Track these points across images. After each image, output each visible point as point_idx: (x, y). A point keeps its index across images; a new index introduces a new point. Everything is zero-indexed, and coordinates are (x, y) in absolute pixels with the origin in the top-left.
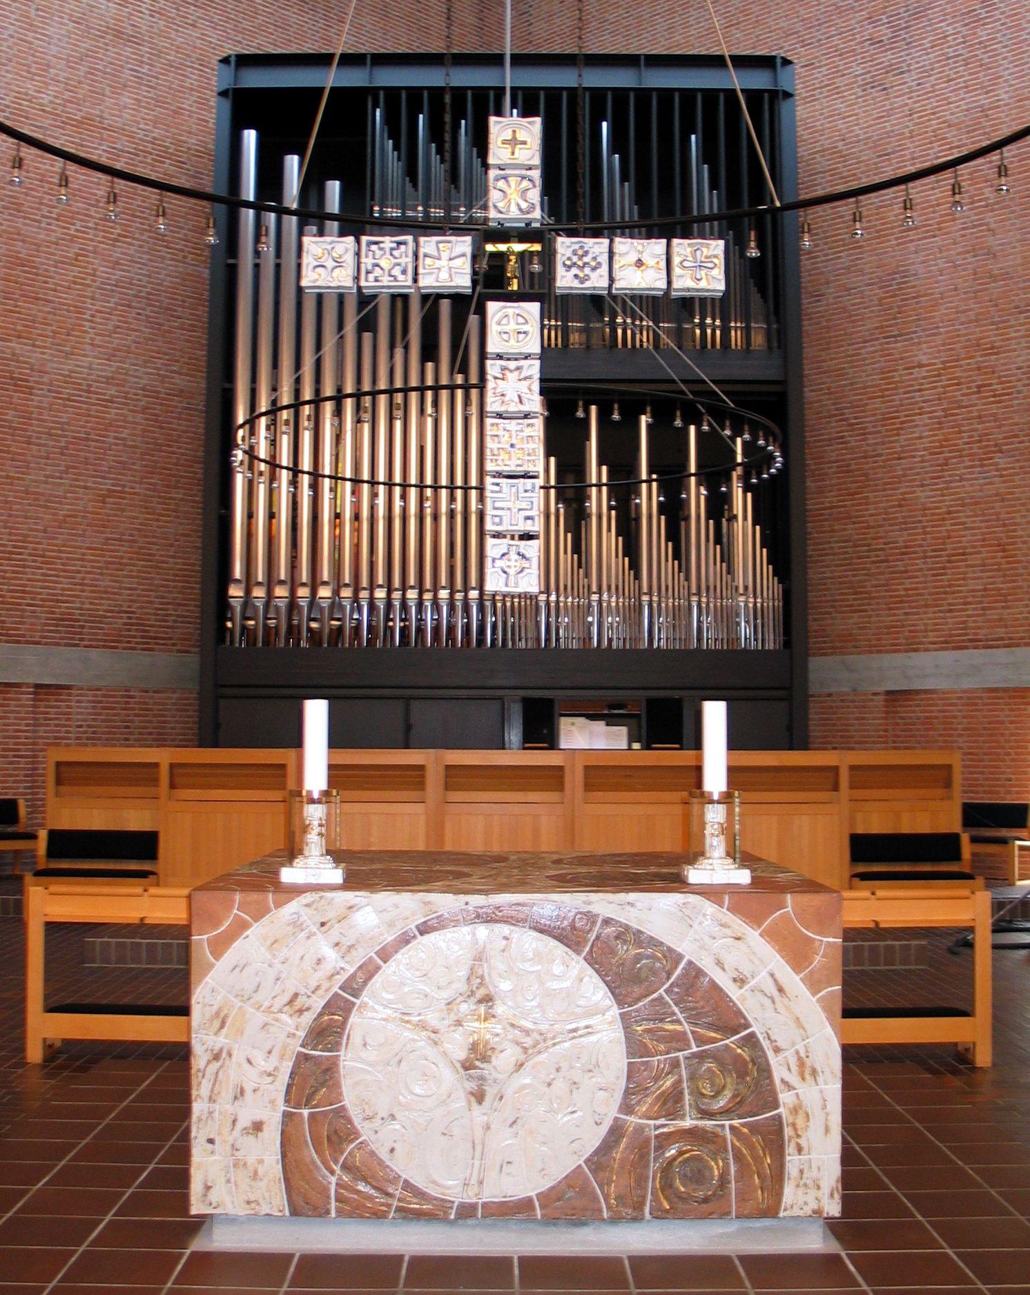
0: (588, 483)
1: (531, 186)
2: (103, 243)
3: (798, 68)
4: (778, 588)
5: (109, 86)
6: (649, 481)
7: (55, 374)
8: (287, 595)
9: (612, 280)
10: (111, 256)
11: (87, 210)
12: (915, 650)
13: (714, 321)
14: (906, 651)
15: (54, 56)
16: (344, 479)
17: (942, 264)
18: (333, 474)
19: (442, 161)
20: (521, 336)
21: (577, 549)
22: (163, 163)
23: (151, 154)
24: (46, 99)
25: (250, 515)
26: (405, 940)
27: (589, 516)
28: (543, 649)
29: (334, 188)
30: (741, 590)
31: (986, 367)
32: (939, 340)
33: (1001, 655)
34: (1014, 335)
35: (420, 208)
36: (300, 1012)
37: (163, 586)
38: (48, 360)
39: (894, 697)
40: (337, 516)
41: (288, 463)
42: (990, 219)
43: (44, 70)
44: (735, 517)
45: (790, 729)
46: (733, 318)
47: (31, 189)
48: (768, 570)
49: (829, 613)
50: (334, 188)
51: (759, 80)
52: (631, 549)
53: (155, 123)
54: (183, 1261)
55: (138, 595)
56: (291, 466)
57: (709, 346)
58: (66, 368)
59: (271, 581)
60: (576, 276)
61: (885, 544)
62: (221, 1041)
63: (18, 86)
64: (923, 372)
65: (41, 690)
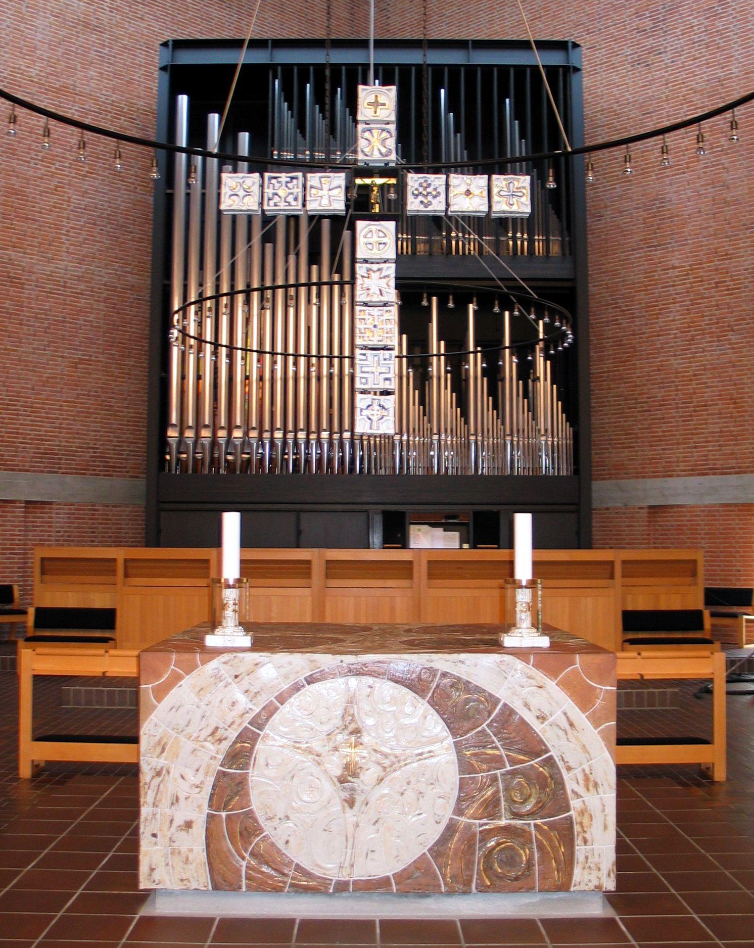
0: (430, 353)
1: (389, 136)
2: (75, 178)
3: (584, 50)
4: (569, 431)
5: (80, 63)
6: (475, 352)
7: (41, 274)
8: (210, 435)
9: (448, 205)
10: (81, 187)
11: (64, 153)
12: (670, 476)
13: (523, 235)
14: (664, 477)
15: (39, 41)
16: (252, 351)
17: (689, 193)
18: (244, 347)
19: (324, 118)
20: (382, 246)
21: (422, 402)
22: (120, 119)
23: (111, 112)
24: (34, 72)
25: (183, 377)
26: (296, 688)
27: (432, 378)
28: (397, 475)
29: (244, 138)
30: (543, 432)
31: (722, 269)
32: (687, 249)
33: (733, 479)
34: (742, 245)
35: (308, 153)
36: (220, 741)
37: (119, 429)
38: (35, 264)
39: (654, 510)
40: (247, 378)
41: (211, 339)
42: (725, 160)
43: (32, 51)
44: (538, 378)
45: (578, 533)
46: (537, 233)
47: (22, 138)
48: (562, 417)
49: (607, 449)
50: (244, 138)
51: (555, 59)
52: (462, 402)
53: (114, 90)
54: (134, 923)
55: (101, 436)
56: (213, 341)
57: (519, 253)
58: (48, 269)
59: (198, 425)
60: (422, 202)
61: (648, 398)
62: (162, 762)
63: (13, 63)
64: (676, 272)
65: (30, 505)
